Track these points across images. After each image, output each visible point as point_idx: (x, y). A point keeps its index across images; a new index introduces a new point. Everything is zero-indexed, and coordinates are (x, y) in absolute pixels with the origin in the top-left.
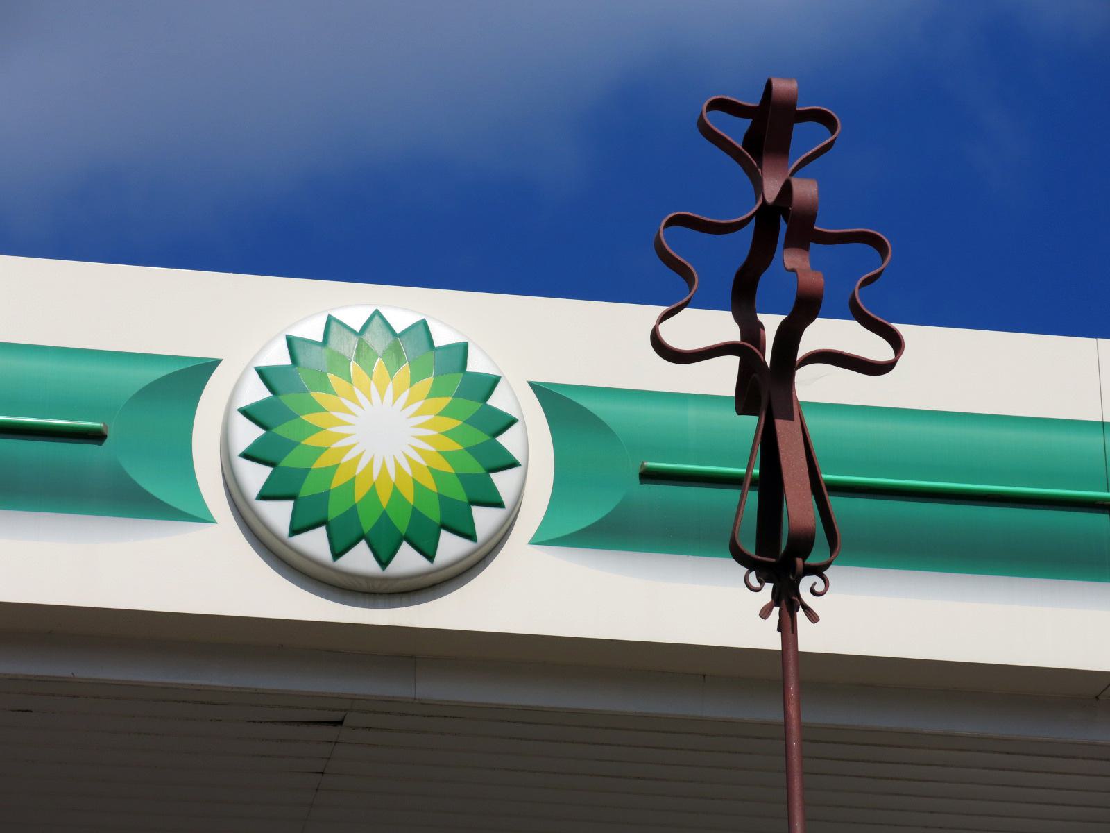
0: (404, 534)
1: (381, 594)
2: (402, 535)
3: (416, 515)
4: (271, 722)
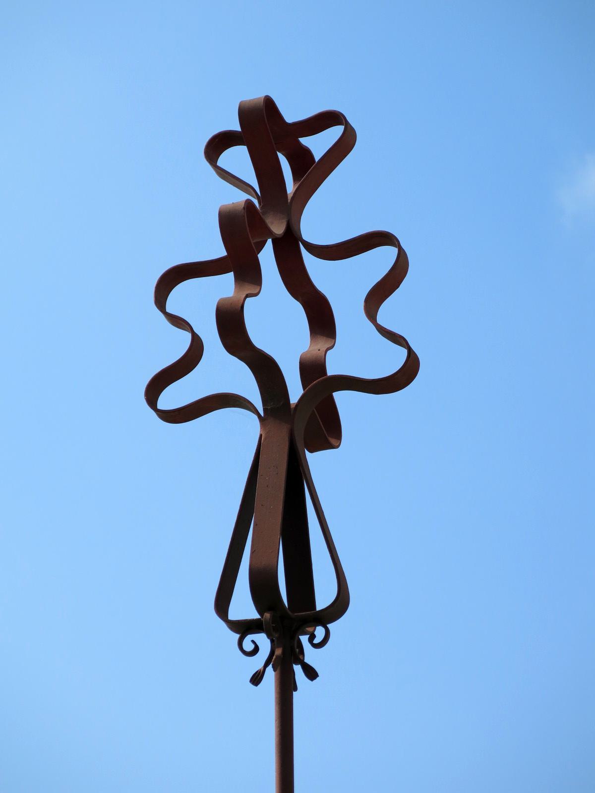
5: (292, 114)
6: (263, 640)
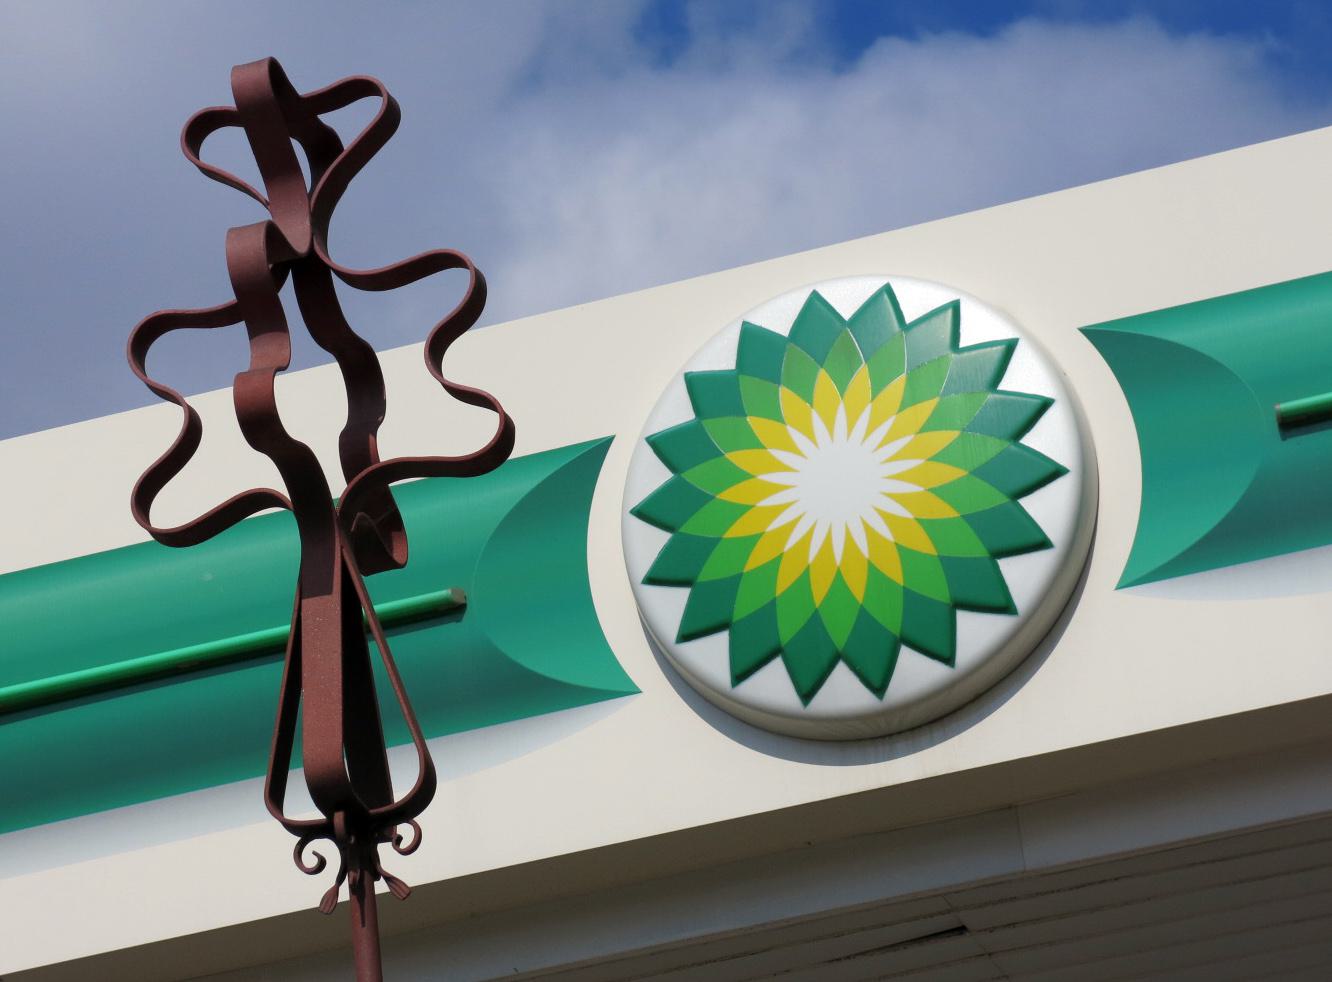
0: (898, 635)
1: (900, 733)
2: (894, 636)
3: (911, 599)
4: (863, 953)
5: (306, 83)
6: (327, 848)
